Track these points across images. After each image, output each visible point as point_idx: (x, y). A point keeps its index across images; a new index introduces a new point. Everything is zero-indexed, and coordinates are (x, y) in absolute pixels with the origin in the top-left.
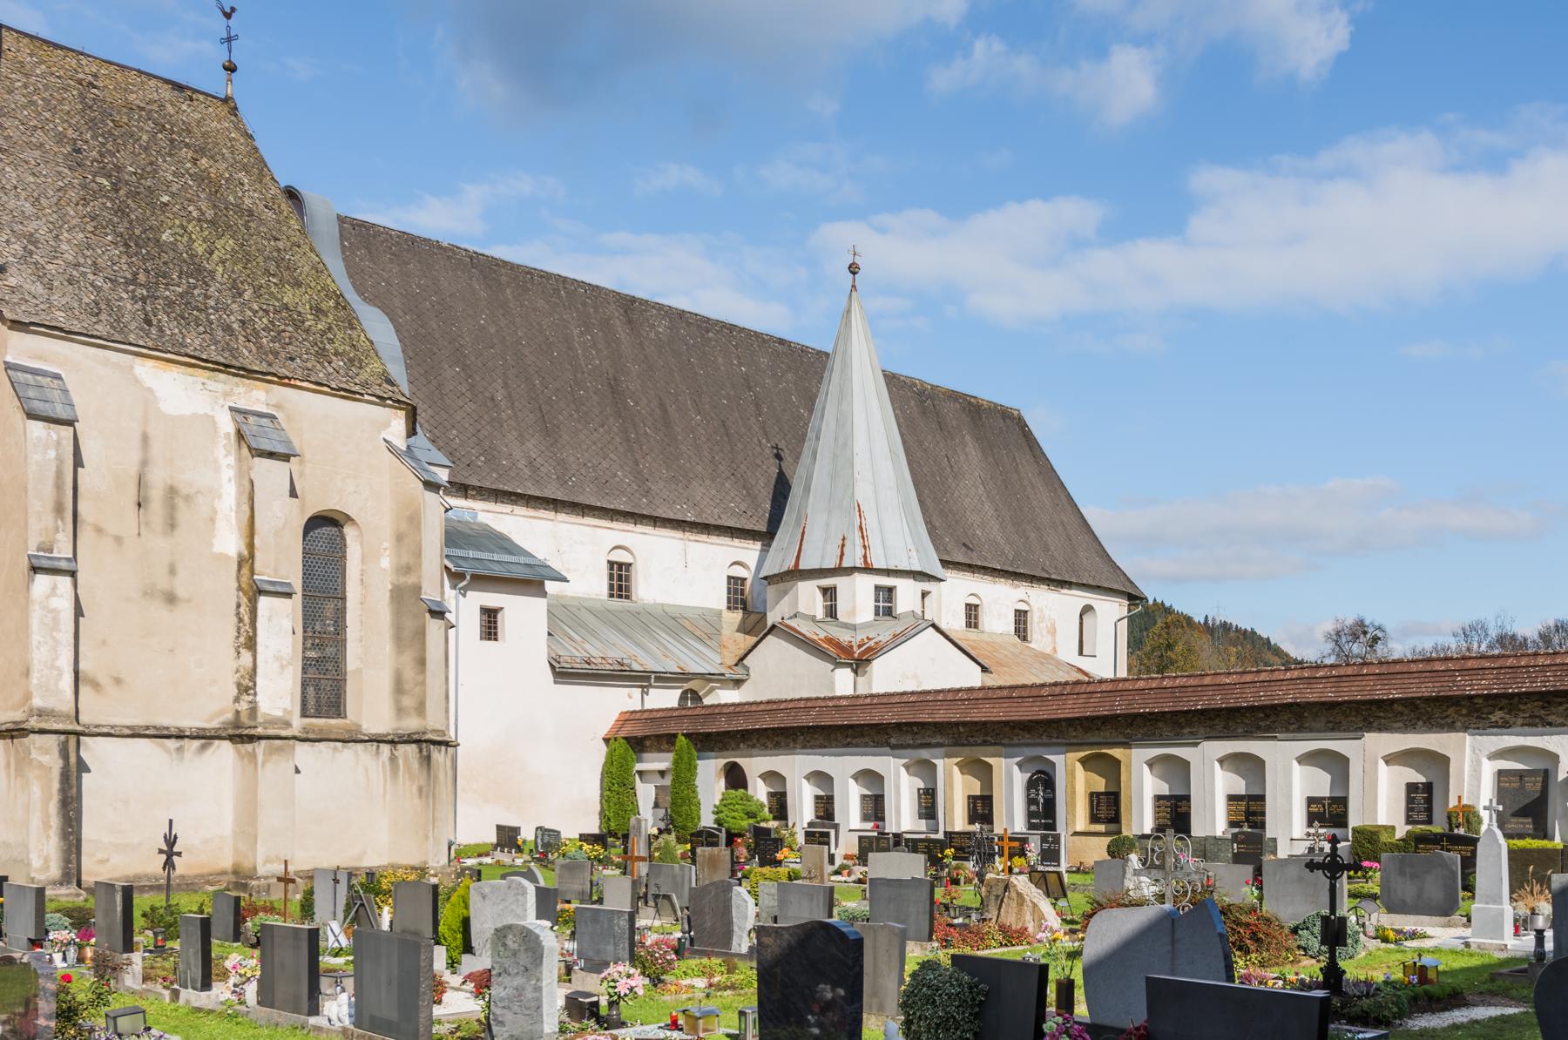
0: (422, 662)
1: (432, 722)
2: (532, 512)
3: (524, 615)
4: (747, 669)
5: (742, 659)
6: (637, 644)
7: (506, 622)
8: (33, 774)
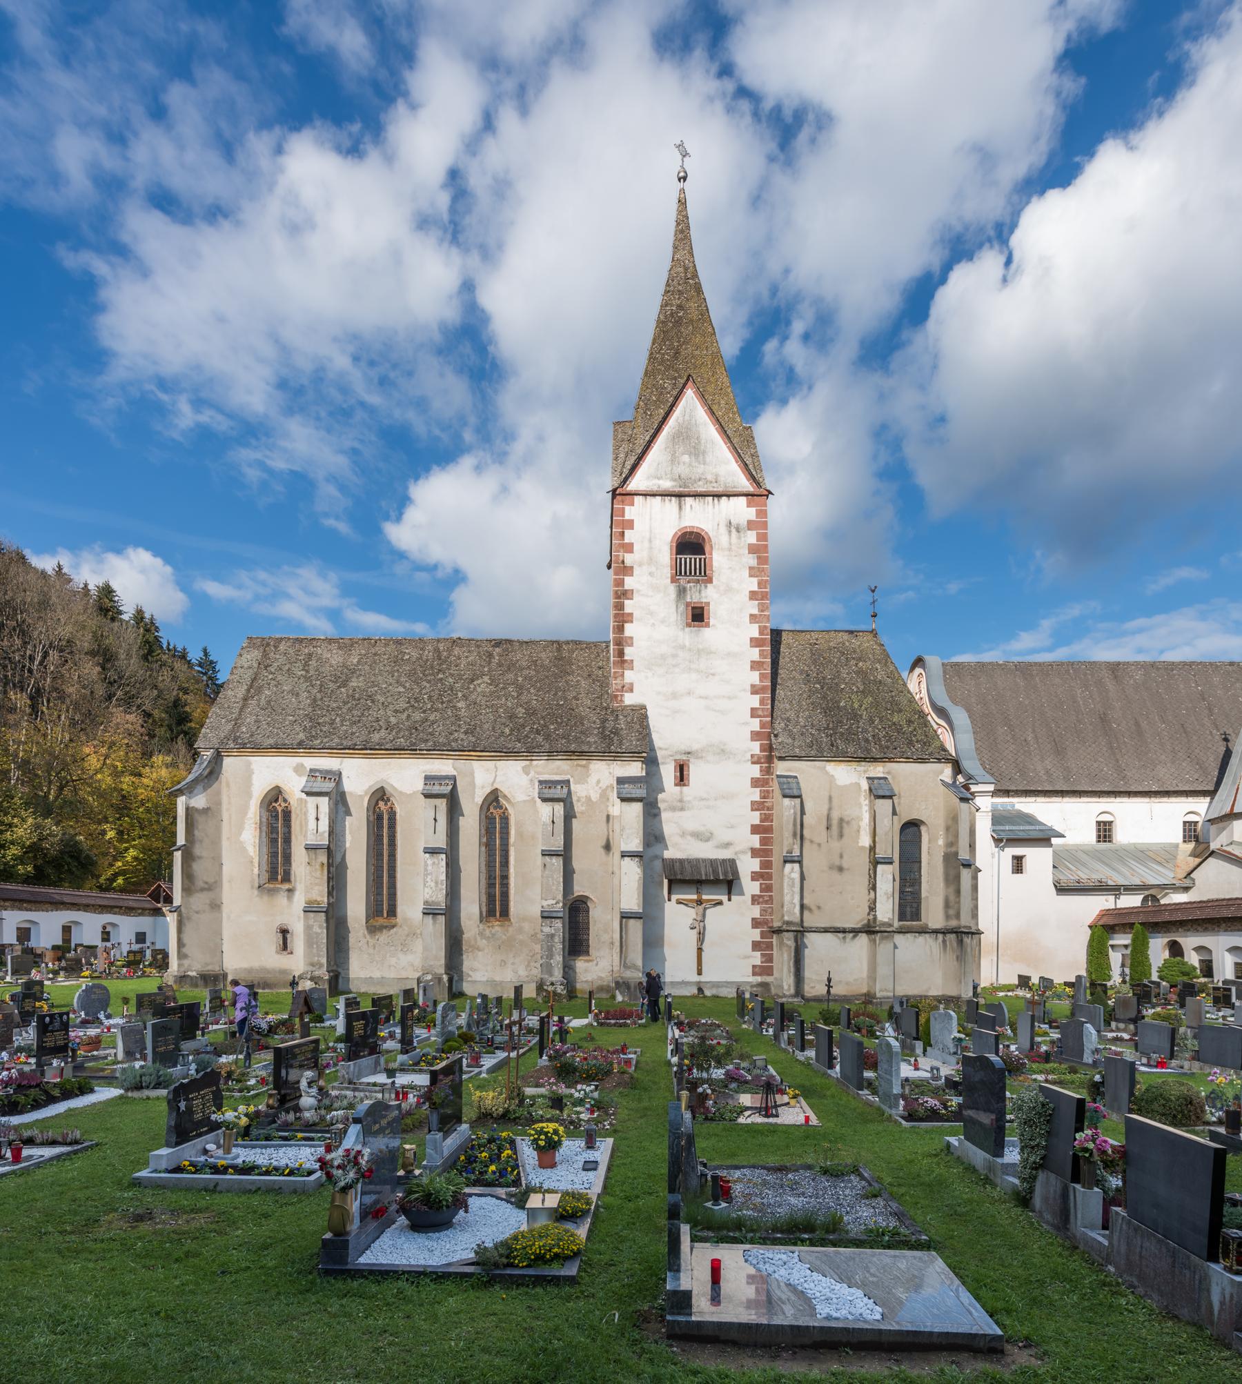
0: (958, 892)
1: (965, 920)
2: (1048, 800)
3: (1038, 859)
4: (1193, 880)
5: (1189, 874)
6: (1114, 869)
7: (1028, 864)
8: (785, 949)
